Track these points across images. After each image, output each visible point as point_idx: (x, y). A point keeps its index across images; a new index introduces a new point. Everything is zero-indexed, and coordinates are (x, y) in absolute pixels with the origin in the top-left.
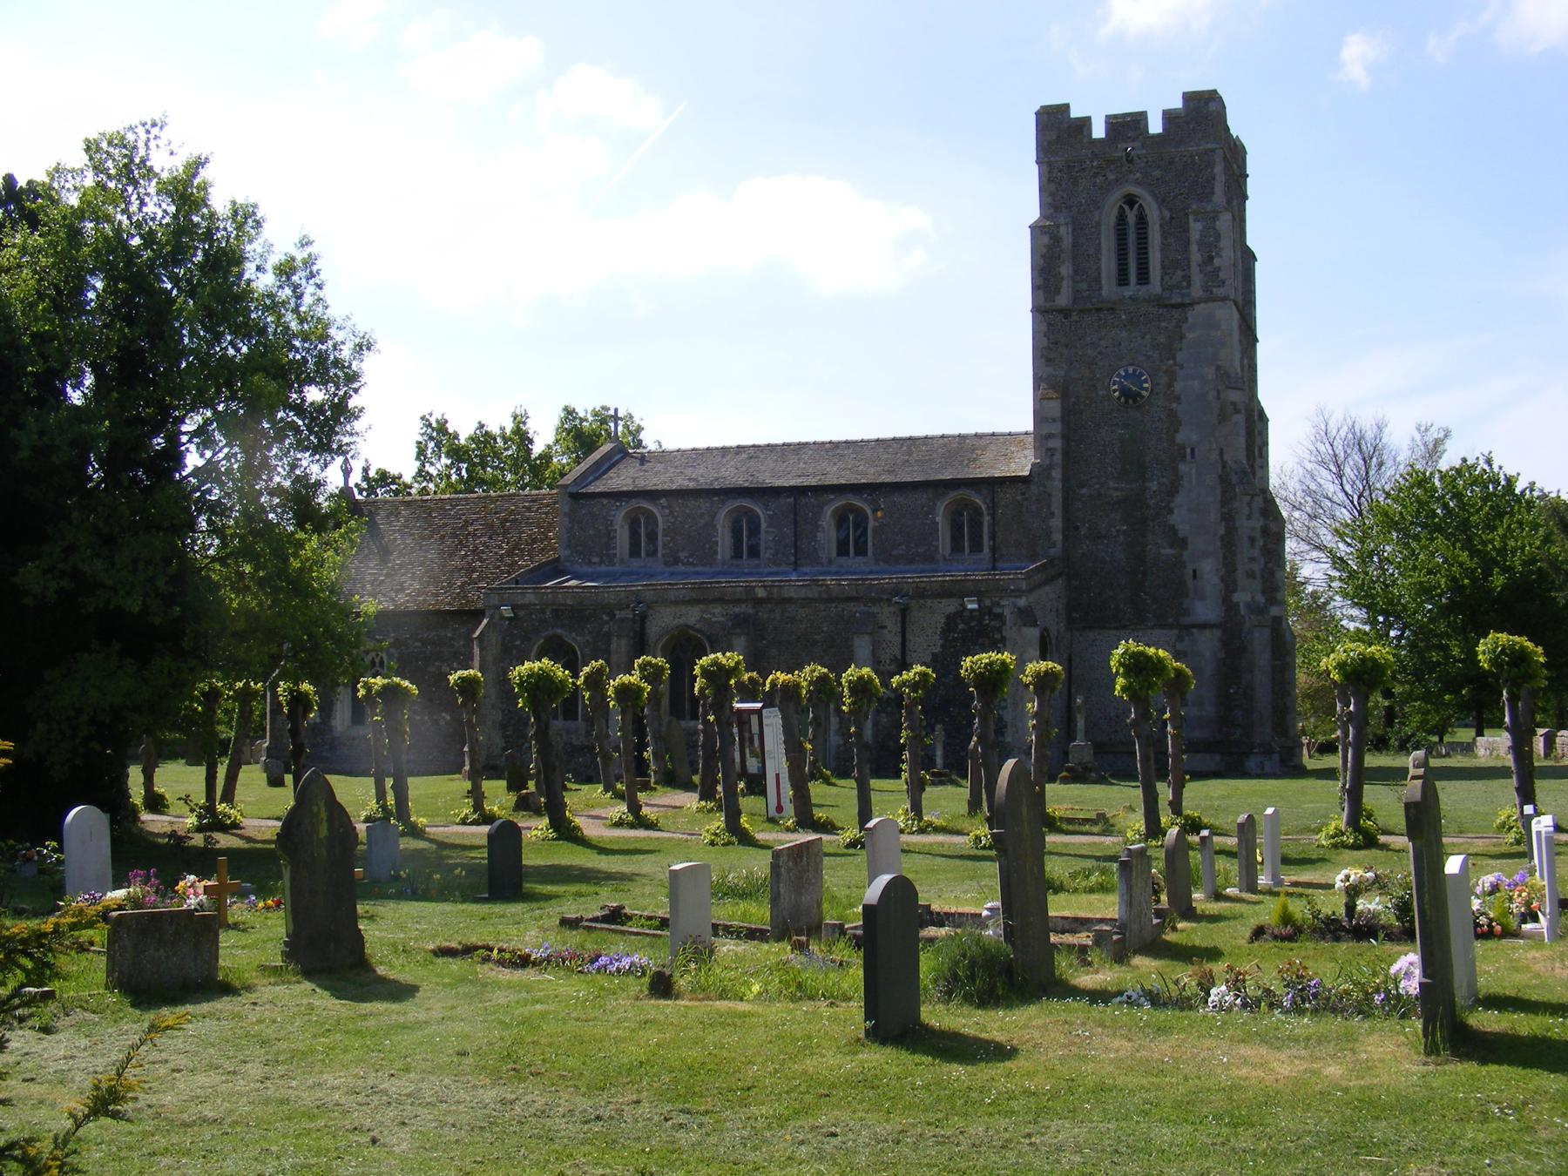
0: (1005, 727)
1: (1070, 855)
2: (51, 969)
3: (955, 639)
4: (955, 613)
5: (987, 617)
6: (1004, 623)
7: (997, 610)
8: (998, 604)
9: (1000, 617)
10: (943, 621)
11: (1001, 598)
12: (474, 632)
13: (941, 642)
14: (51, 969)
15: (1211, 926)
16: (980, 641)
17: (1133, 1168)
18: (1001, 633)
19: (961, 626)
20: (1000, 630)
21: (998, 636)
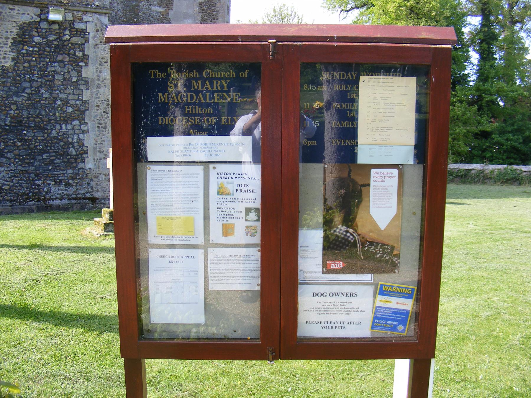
0: (86, 152)
1: (57, 249)
2: (249, 79)
3: (29, 54)
4: (30, 24)
5: (67, 32)
6: (87, 41)
7: (79, 26)
8: (81, 20)
9: (83, 33)
10: (15, 31)
11: (85, 13)
12: (259, 344)
13: (13, 55)
14: (249, 79)
15: (30, 251)
16: (60, 58)
17: (54, 397)
18: (83, 51)
19: (37, 39)
20: (82, 48)
21: (79, 54)
